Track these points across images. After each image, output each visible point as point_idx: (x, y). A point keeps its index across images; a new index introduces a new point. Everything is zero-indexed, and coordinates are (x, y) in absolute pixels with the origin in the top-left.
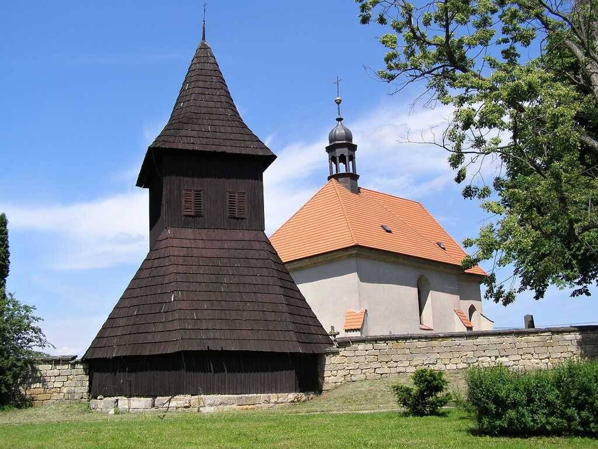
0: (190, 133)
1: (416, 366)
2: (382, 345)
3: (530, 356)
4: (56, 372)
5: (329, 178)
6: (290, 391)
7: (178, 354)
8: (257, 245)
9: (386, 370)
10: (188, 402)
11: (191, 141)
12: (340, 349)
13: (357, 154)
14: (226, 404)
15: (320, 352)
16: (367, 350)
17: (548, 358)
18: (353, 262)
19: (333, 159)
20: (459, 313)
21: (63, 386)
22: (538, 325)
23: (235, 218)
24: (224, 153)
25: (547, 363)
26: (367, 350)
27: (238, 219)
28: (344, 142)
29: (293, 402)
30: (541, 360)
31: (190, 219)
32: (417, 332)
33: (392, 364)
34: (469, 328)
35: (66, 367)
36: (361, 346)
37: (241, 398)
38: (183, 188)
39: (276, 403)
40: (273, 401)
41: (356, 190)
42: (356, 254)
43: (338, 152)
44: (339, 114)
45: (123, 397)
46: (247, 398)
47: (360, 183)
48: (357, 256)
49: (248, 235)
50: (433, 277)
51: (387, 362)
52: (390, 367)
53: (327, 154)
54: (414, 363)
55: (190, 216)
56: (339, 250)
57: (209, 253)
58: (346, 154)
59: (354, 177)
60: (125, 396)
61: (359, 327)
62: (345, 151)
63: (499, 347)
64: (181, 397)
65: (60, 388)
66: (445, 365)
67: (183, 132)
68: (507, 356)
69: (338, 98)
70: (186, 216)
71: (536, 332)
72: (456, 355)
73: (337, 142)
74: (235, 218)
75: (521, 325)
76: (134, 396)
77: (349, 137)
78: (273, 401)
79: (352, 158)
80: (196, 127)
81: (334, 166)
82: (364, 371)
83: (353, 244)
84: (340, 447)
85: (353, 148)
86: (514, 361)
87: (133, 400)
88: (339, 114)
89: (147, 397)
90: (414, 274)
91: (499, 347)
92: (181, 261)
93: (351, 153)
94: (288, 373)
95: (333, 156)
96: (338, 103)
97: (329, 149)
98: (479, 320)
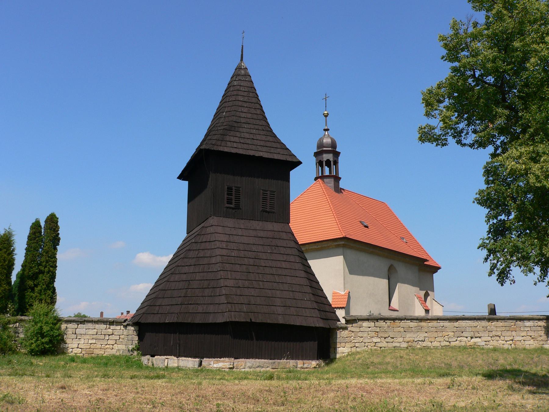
0: (232, 139)
1: (408, 342)
2: (381, 323)
3: (498, 338)
4: (110, 331)
5: (316, 179)
6: (313, 359)
7: (225, 324)
8: (284, 236)
9: (384, 344)
10: (232, 364)
11: (232, 146)
12: (348, 326)
13: (341, 159)
14: (263, 367)
15: (334, 327)
16: (369, 327)
17: (512, 340)
18: (341, 250)
19: (320, 163)
20: (419, 298)
21: (116, 343)
22: (500, 313)
23: (266, 212)
24: (261, 158)
25: (511, 345)
26: (369, 327)
27: (269, 212)
28: (330, 149)
29: (315, 367)
30: (506, 341)
31: (230, 210)
32: (387, 313)
33: (389, 339)
34: (427, 311)
35: (118, 327)
36: (365, 324)
37: (274, 363)
38: (217, 181)
39: (302, 368)
40: (299, 366)
41: (338, 190)
42: (343, 244)
43: (326, 157)
44: (326, 125)
45: (173, 357)
46: (279, 363)
47: (342, 185)
48: (344, 246)
49: (277, 226)
50: (401, 269)
51: (385, 338)
52: (387, 342)
53: (314, 158)
54: (407, 339)
55: (230, 208)
56: (331, 239)
57: (245, 240)
58: (331, 160)
59: (337, 179)
60: (175, 356)
61: (345, 306)
62: (330, 157)
63: (474, 329)
64: (227, 359)
65: (113, 345)
66: (431, 342)
67: (228, 138)
68: (480, 337)
69: (326, 112)
70: (227, 208)
71: (498, 320)
72: (440, 335)
73: (324, 149)
74: (266, 212)
75: (485, 312)
76: (182, 356)
77: (333, 145)
78: (299, 366)
79: (336, 163)
80: (238, 134)
81: (320, 168)
82: (366, 344)
83: (342, 236)
84: (429, 407)
85: (337, 154)
86: (485, 341)
87: (182, 360)
88: (326, 125)
89: (195, 357)
90: (383, 264)
91: (474, 329)
92: (224, 246)
93: (335, 159)
94: (312, 343)
95: (320, 161)
96: (326, 116)
97: (316, 154)
98: (432, 304)
